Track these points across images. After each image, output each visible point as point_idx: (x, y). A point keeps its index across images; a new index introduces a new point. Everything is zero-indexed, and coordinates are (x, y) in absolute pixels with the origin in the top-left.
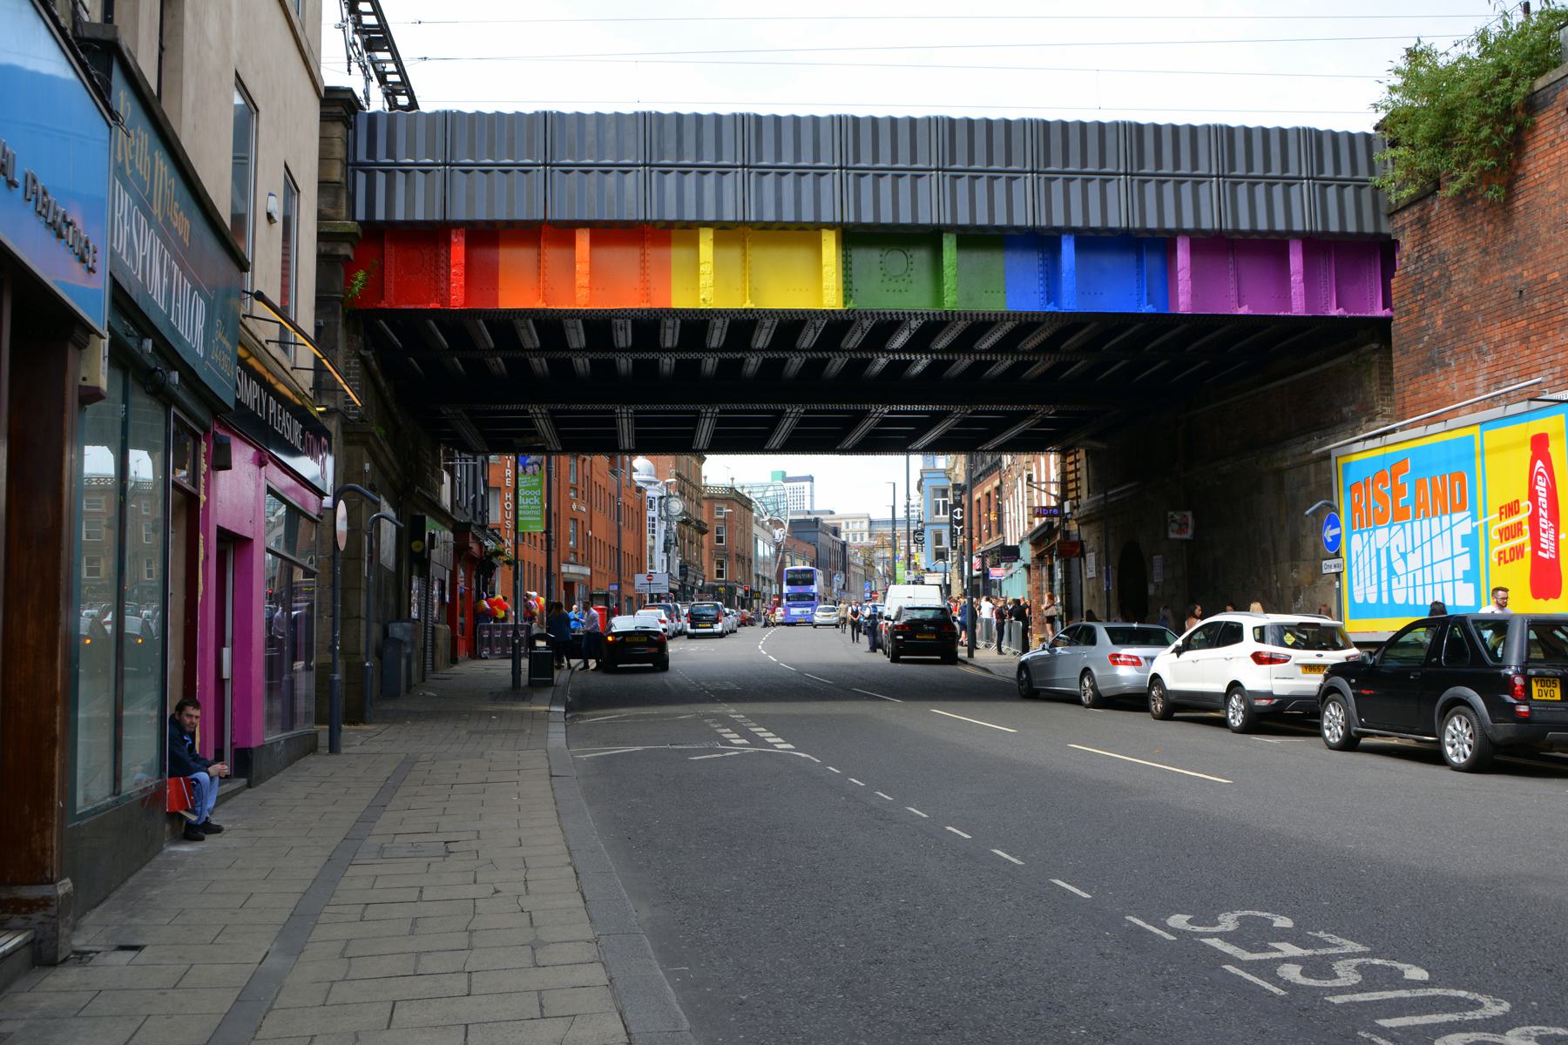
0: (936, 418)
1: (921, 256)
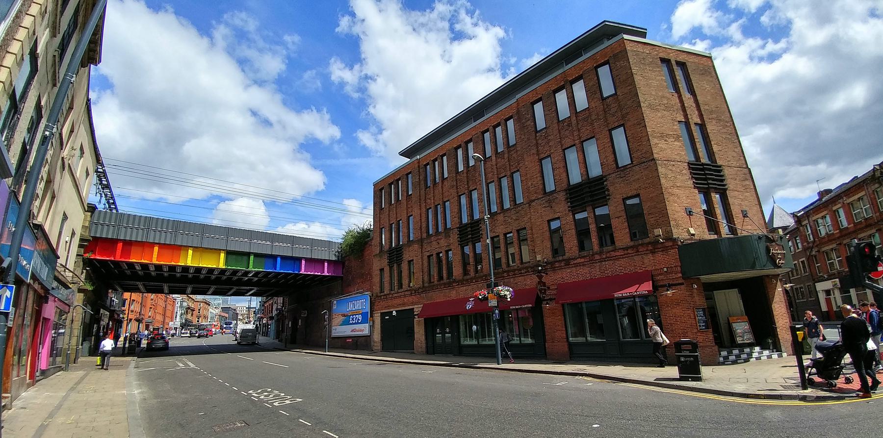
0: (251, 290)
1: (245, 258)
